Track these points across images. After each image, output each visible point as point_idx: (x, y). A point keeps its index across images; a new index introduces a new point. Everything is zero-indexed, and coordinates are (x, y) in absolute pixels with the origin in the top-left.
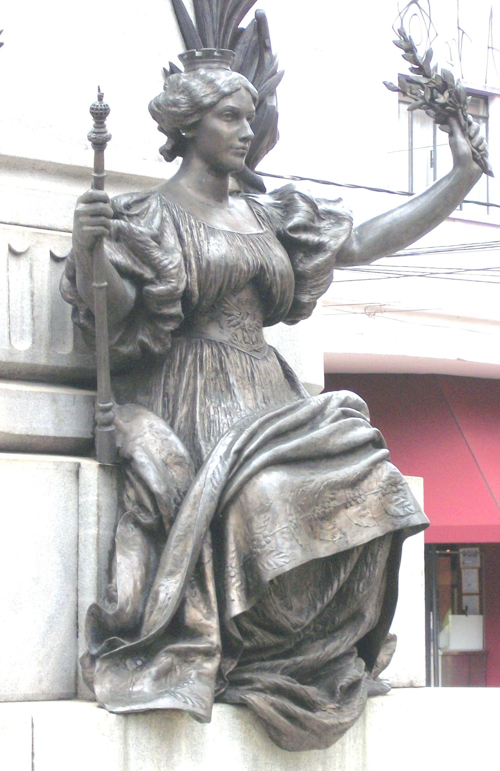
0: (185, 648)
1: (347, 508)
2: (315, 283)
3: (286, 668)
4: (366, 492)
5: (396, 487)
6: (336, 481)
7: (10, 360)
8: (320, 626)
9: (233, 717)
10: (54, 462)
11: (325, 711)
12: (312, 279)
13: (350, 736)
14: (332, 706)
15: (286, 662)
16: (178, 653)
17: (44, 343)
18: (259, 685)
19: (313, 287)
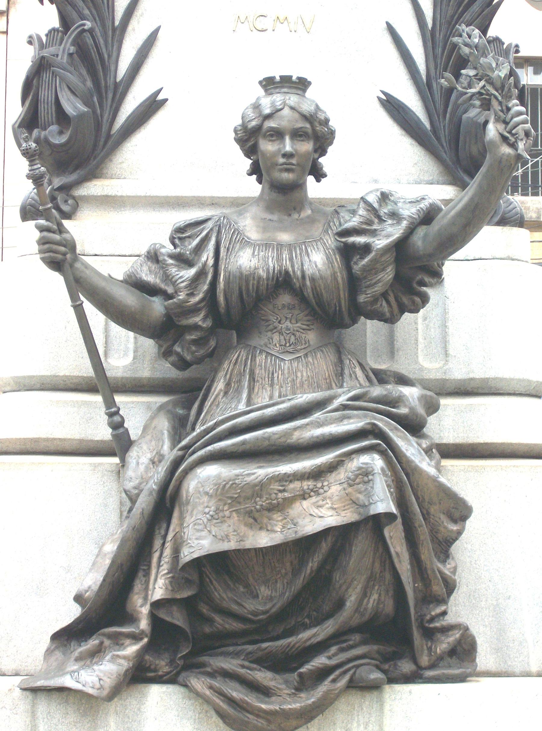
0: (112, 632)
1: (305, 499)
2: (368, 283)
3: (250, 653)
4: (332, 483)
5: (368, 477)
6: (285, 473)
7: (133, 375)
8: (315, 613)
9: (183, 698)
10: (91, 464)
11: (280, 696)
12: (366, 279)
13: (358, 721)
14: (286, 692)
15: (250, 648)
16: (110, 636)
17: (148, 358)
18: (209, 669)
19: (368, 287)
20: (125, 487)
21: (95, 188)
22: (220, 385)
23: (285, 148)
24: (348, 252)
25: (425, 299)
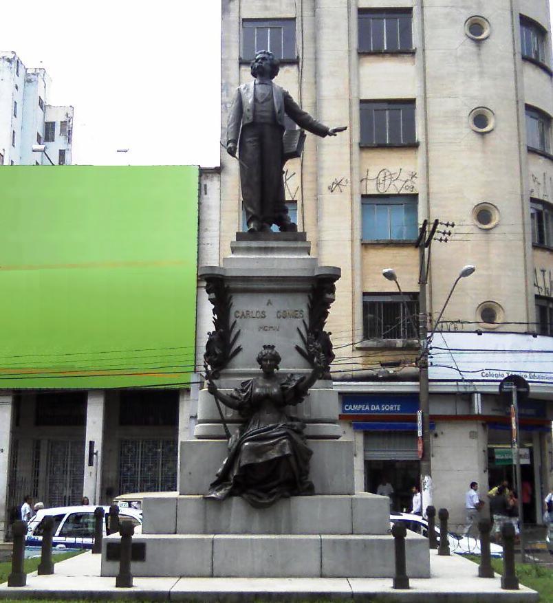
20: (208, 489)
21: (224, 371)
22: (252, 422)
23: (269, 361)
24: (283, 389)
25: (303, 400)
